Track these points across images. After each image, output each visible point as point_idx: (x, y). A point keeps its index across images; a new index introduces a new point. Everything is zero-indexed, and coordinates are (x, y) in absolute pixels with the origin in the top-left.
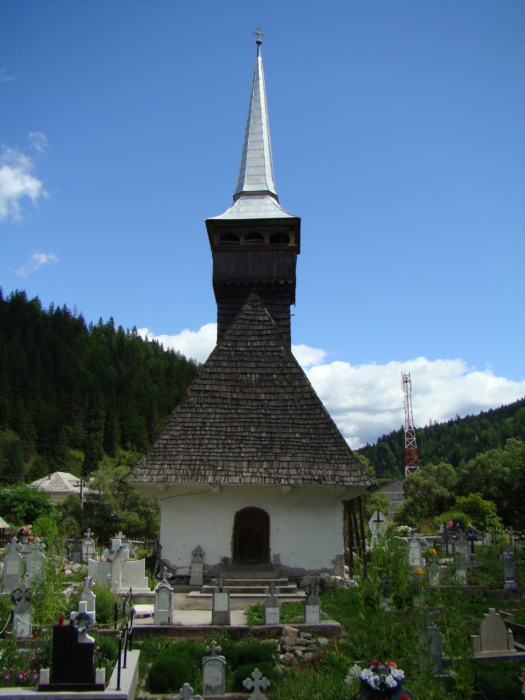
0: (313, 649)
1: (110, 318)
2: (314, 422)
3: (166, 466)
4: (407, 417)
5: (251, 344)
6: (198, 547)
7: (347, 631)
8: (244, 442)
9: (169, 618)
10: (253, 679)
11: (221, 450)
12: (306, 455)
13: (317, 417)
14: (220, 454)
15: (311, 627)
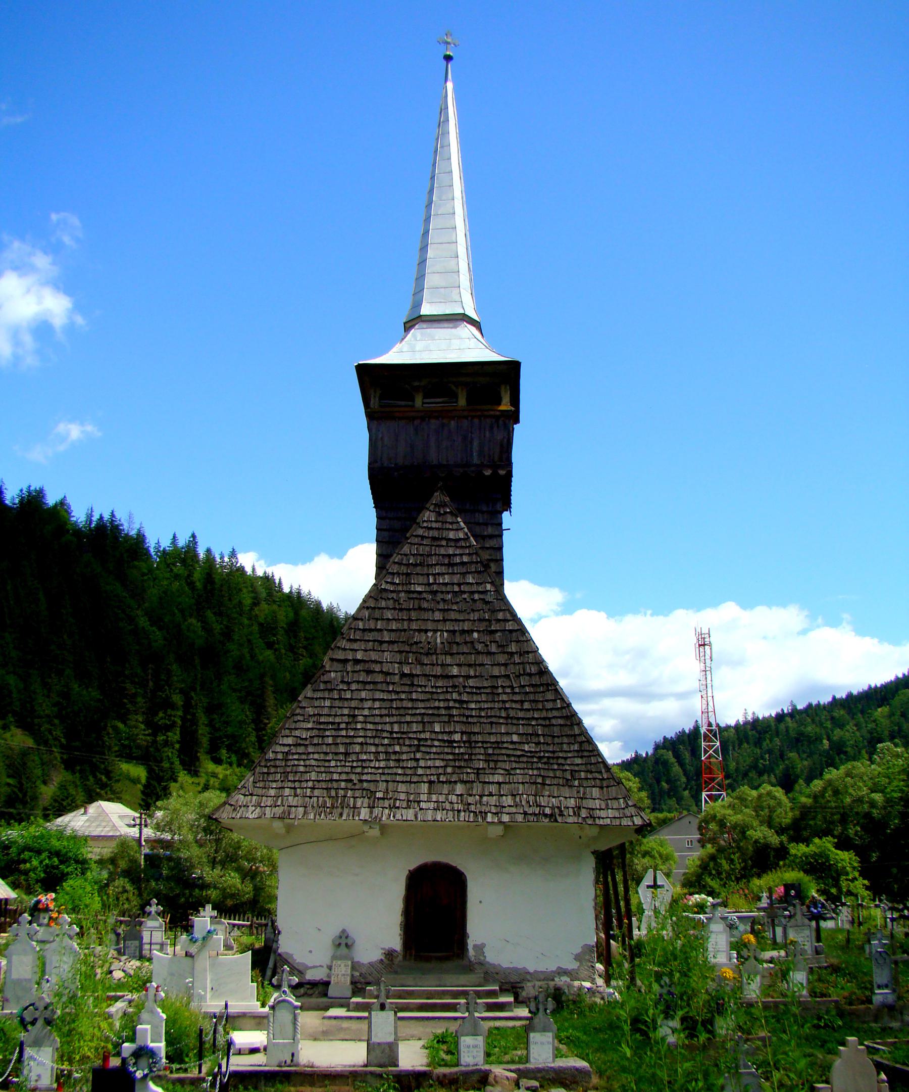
1: (190, 535)
3: (287, 792)
4: (704, 706)
5: (435, 580)
6: (344, 931)
9: (293, 1055)
13: (549, 705)
14: (380, 771)
15: (539, 1070)
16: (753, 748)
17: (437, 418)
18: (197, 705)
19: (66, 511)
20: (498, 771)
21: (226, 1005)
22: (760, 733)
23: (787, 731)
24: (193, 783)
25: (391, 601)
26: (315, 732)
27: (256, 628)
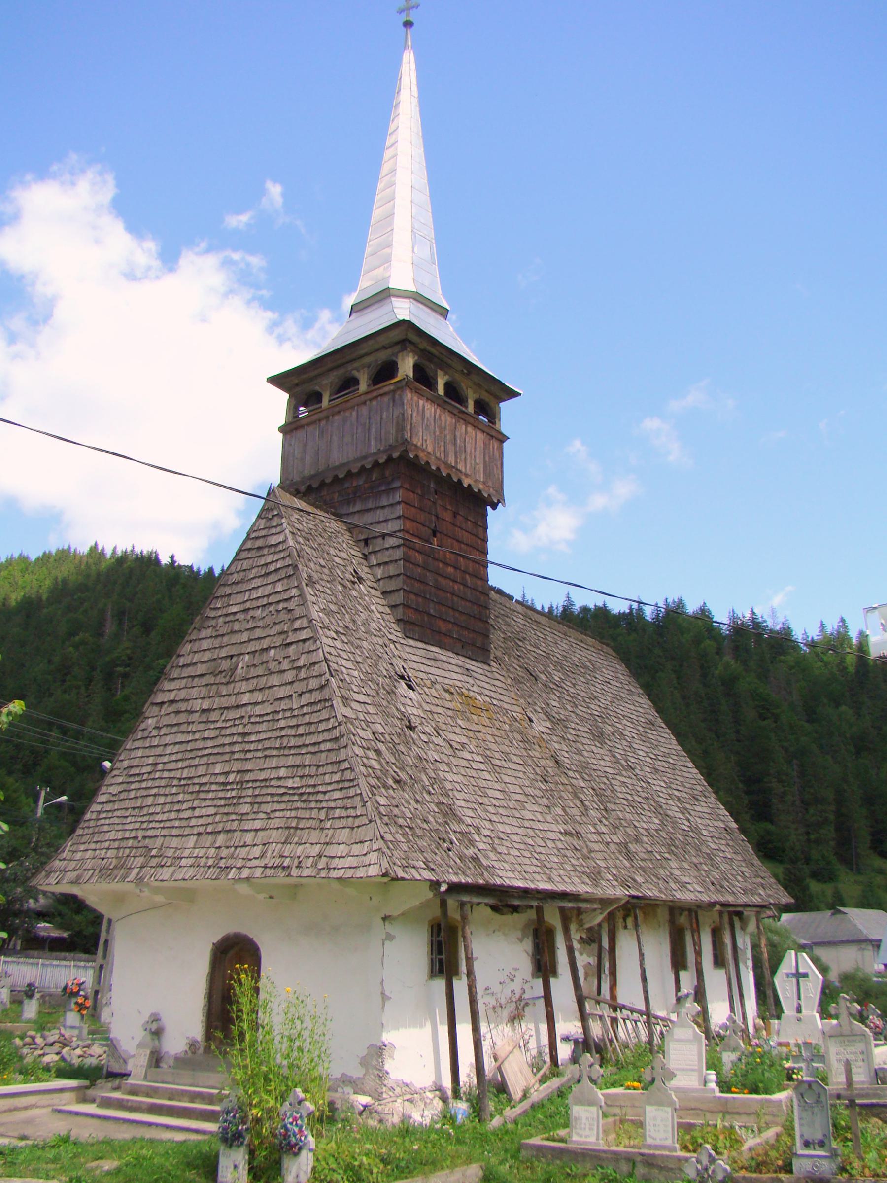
1: (838, 620)
19: (708, 617)
24: (856, 882)
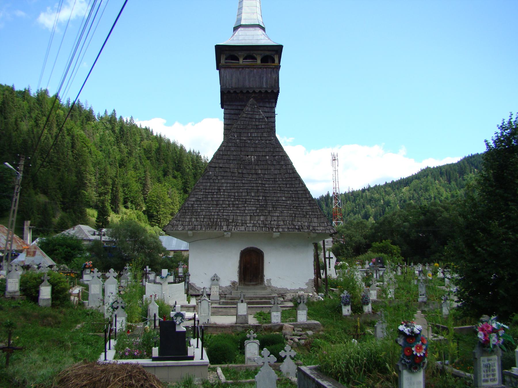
0: (304, 338)
2: (295, 189)
3: (193, 220)
4: (335, 186)
5: (251, 135)
6: (215, 274)
7: (323, 327)
8: (247, 203)
9: (208, 320)
10: (285, 351)
11: (231, 209)
12: (290, 212)
13: (297, 186)
14: (230, 211)
15: (301, 324)
16: (351, 203)
17: (248, 68)
18: (118, 184)
20: (277, 212)
21: (176, 302)
22: (355, 197)
23: (366, 196)
25: (234, 144)
26: (204, 196)
27: (142, 151)
